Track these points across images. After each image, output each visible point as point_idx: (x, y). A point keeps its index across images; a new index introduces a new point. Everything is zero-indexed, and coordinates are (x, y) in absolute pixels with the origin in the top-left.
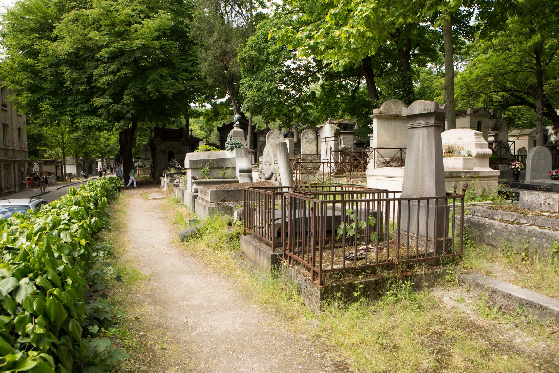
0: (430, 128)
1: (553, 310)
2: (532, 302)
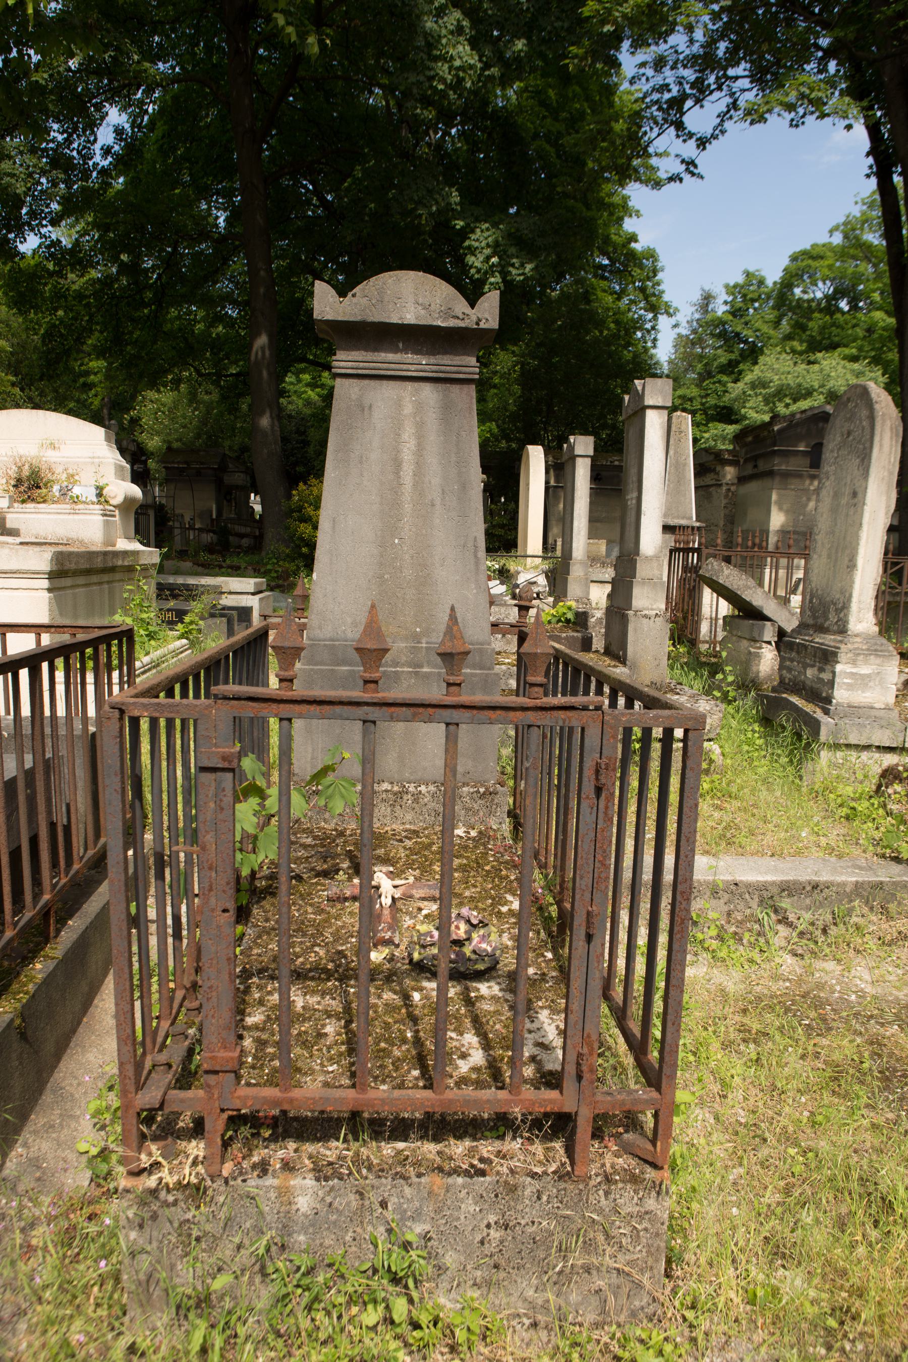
0: (455, 389)
1: (844, 884)
2: (795, 882)
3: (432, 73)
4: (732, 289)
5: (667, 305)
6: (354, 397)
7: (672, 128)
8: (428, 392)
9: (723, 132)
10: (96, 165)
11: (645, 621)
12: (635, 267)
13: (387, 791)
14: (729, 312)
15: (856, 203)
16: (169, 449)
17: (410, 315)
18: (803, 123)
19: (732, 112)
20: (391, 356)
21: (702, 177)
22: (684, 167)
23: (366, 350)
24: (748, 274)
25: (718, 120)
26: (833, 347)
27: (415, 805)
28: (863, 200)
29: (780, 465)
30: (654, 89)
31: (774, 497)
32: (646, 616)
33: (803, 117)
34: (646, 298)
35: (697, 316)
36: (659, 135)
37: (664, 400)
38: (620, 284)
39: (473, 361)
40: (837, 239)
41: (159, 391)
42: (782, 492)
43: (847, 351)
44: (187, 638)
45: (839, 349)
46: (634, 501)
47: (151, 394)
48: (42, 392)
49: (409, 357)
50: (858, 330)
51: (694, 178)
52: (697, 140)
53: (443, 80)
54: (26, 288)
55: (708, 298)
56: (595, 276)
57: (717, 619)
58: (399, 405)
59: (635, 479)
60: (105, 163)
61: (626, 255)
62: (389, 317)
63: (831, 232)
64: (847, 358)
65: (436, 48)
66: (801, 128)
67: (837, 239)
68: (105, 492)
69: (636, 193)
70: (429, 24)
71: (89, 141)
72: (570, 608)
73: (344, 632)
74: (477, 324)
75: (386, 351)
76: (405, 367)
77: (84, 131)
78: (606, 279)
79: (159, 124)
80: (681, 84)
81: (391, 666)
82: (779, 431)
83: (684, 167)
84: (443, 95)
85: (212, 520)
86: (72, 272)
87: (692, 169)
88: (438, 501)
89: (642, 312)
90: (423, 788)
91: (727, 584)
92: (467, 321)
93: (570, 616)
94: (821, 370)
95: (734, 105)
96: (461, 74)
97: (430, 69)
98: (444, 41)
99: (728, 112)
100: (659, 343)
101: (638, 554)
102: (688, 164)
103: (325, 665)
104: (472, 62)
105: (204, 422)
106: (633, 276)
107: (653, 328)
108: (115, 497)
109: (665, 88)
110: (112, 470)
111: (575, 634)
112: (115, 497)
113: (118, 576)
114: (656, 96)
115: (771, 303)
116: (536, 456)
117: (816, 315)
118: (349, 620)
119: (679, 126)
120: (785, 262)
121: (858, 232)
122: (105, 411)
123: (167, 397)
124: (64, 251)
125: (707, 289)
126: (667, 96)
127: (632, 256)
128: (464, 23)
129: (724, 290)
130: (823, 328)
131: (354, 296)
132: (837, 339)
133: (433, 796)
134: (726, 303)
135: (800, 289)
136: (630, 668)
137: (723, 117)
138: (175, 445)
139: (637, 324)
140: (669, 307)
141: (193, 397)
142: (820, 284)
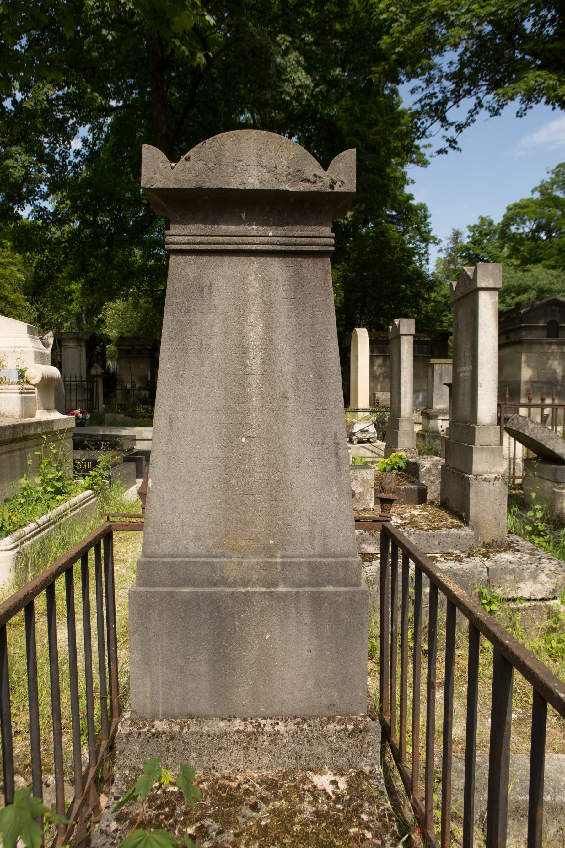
0: (308, 263)
3: (281, 90)
4: (472, 229)
5: (434, 238)
6: (191, 276)
7: (438, 121)
8: (276, 267)
9: (473, 121)
10: (70, 162)
11: (485, 484)
12: (413, 217)
13: (239, 732)
14: (470, 242)
15: (548, 173)
16: (121, 338)
17: (253, 180)
18: (525, 114)
19: (478, 109)
20: (232, 229)
21: (460, 150)
22: (448, 144)
23: (204, 223)
24: (482, 219)
25: (469, 115)
26: (538, 261)
27: (272, 747)
28: (552, 171)
29: (525, 336)
30: (426, 97)
31: (524, 358)
32: (486, 480)
33: (525, 110)
34: (421, 234)
35: (451, 245)
36: (432, 124)
37: (495, 283)
38: (403, 227)
39: (327, 231)
40: (537, 196)
41: (115, 302)
42: (529, 354)
43: (548, 263)
44: (92, 489)
45: (543, 262)
46: (467, 374)
47: (111, 304)
48: (45, 305)
49: (254, 229)
50: (553, 250)
51: (455, 151)
52: (456, 126)
53: (289, 94)
54: (26, 239)
55: (457, 234)
56: (387, 222)
57: (514, 458)
58: (243, 282)
59: (468, 354)
60: (77, 161)
61: (406, 208)
62: (228, 183)
63: (533, 192)
64: (546, 266)
65: (283, 74)
66: (524, 117)
67: (537, 196)
68: (26, 374)
69: (411, 170)
70: (279, 60)
71: (67, 148)
72: (401, 458)
73: (185, 546)
74: (332, 187)
75: (227, 223)
76: (249, 240)
77: (64, 141)
78: (394, 223)
79: (111, 138)
80: (443, 92)
81: (240, 585)
82: (524, 313)
83: (448, 144)
84: (289, 103)
85: (147, 382)
86: (54, 226)
87: (453, 145)
88: (291, 393)
89: (418, 243)
90: (281, 727)
91: (533, 436)
92: (319, 184)
93: (402, 464)
94: (533, 275)
95: (479, 104)
96: (300, 90)
97: (280, 87)
98: (289, 69)
99: (476, 109)
100: (430, 261)
101: (476, 423)
102: (451, 142)
103: (164, 585)
104: (308, 82)
105: (144, 320)
106: (411, 221)
107: (426, 252)
108: (34, 378)
109: (433, 95)
110: (32, 357)
111: (412, 486)
112: (34, 378)
113: (30, 443)
114: (427, 101)
115: (497, 236)
116: (362, 336)
117: (526, 242)
118: (191, 533)
119: (443, 119)
120: (505, 211)
121: (549, 191)
122: (83, 316)
123: (119, 304)
124: (48, 214)
125: (456, 228)
126: (435, 101)
127: (411, 208)
128: (300, 59)
129: (467, 230)
130: (530, 251)
131: (187, 160)
132: (540, 256)
133: (293, 736)
134: (469, 237)
135: (515, 226)
136: (473, 529)
137: (472, 113)
138: (126, 335)
139: (412, 253)
140: (436, 239)
141: (136, 305)
142: (528, 223)
